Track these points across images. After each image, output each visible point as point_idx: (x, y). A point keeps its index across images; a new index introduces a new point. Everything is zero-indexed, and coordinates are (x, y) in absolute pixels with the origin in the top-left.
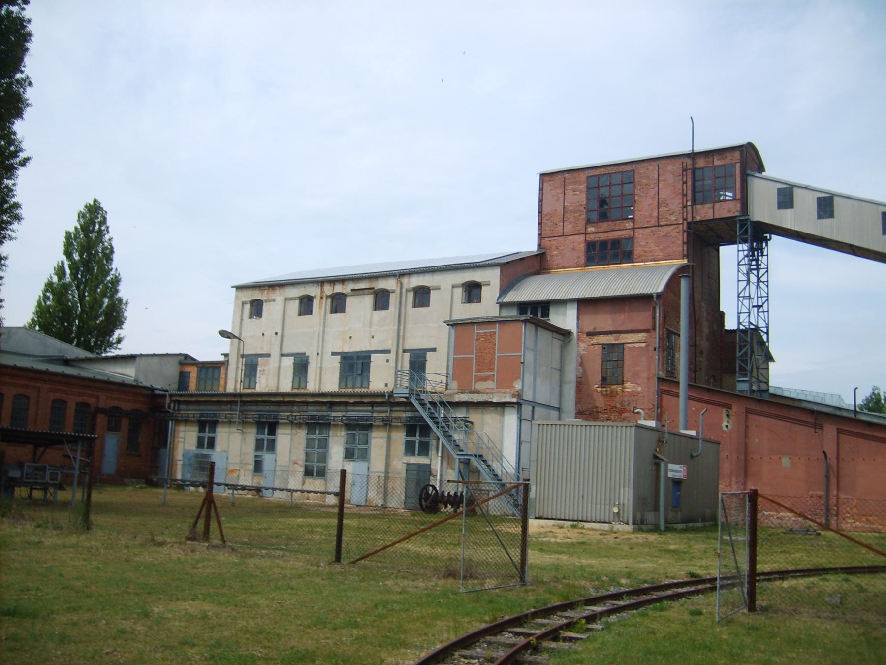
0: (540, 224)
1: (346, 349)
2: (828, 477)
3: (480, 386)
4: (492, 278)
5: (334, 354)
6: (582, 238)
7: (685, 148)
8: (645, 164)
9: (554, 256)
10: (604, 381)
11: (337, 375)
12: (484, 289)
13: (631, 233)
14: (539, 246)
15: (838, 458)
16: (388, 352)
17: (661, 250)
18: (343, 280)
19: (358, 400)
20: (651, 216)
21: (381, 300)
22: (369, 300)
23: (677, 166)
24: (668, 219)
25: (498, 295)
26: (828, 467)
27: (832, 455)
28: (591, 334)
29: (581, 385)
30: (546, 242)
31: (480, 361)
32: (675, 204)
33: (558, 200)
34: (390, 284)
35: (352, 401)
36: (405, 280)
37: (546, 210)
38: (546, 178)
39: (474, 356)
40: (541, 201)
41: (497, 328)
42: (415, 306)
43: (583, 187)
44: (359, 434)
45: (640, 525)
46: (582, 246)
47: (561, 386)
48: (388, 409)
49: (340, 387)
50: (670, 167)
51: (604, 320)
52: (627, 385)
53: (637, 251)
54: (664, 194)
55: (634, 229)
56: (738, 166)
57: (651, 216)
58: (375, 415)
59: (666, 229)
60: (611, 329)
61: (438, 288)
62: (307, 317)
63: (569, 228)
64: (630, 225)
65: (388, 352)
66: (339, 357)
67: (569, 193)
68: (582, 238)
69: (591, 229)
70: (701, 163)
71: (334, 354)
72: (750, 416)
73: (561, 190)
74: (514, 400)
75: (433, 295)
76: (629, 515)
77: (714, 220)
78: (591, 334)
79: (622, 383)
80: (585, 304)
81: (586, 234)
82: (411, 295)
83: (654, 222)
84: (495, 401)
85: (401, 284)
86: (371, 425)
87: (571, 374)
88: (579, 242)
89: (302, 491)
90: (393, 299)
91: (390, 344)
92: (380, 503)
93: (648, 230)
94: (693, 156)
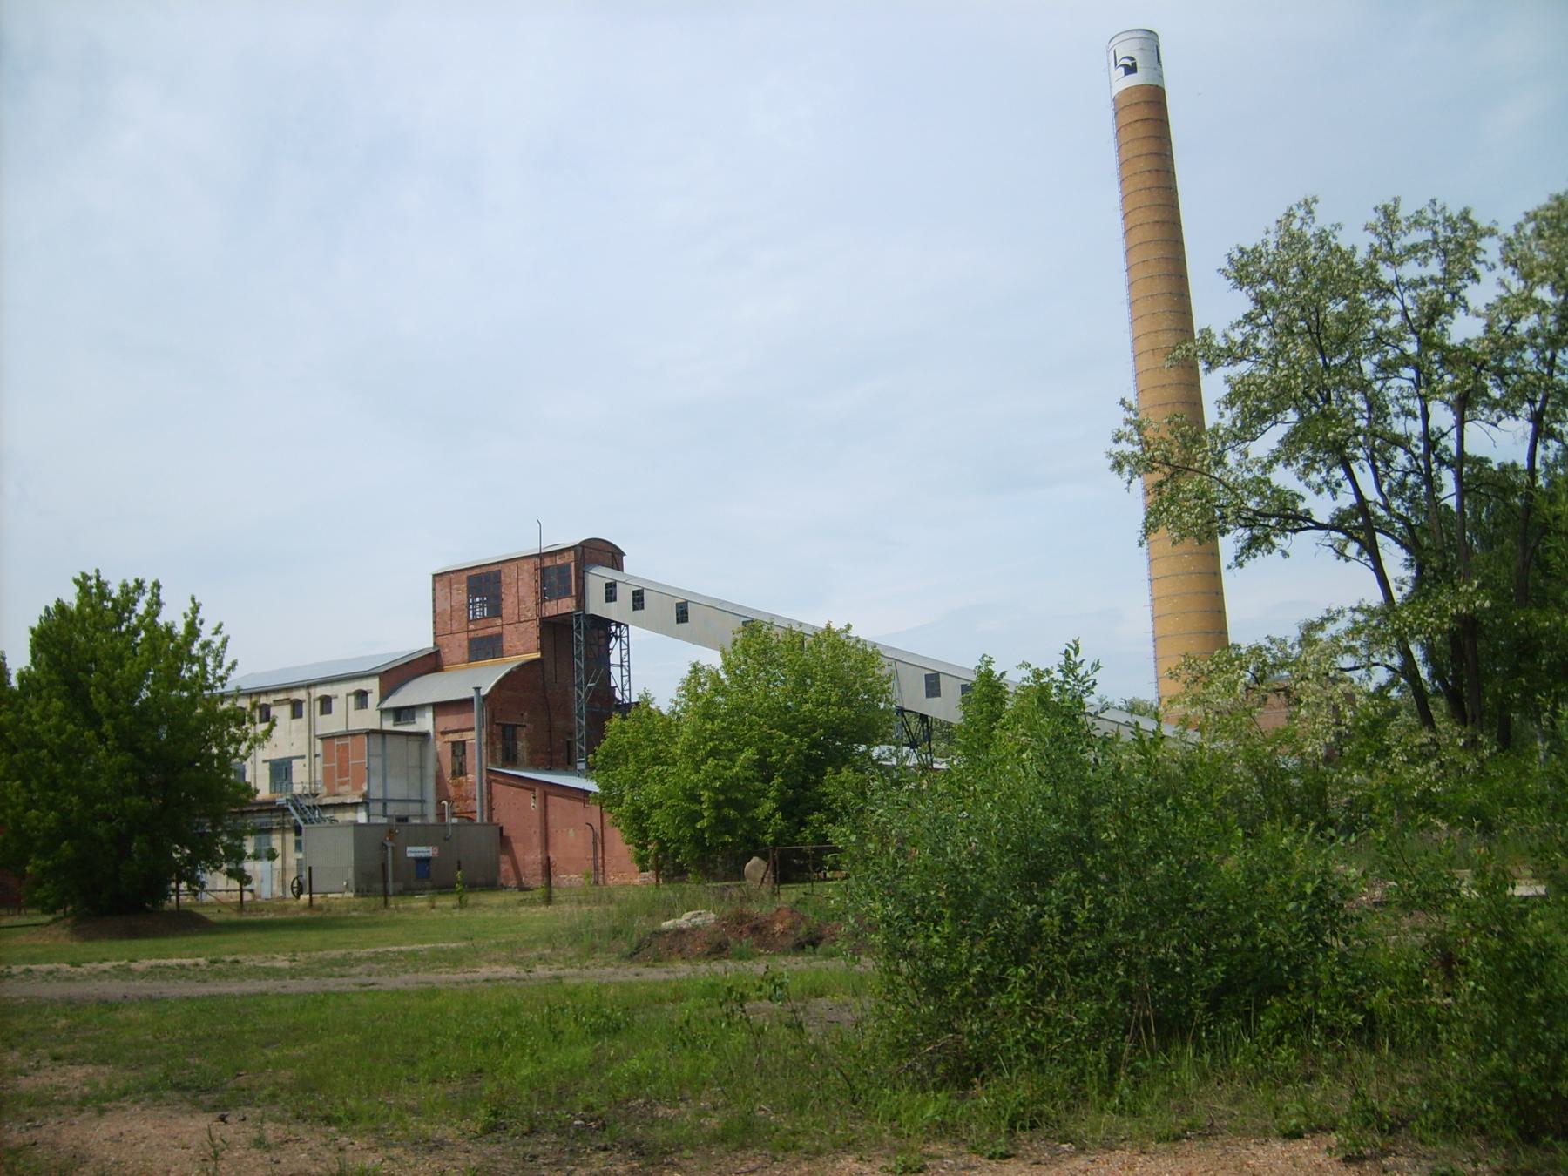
0: (434, 622)
1: (273, 757)
2: (595, 843)
3: (342, 789)
4: (373, 685)
5: (265, 761)
6: (464, 635)
7: (533, 549)
8: (508, 564)
9: (447, 657)
10: (454, 773)
11: (268, 781)
12: (333, 701)
13: (499, 629)
14: (435, 643)
15: (602, 827)
16: (303, 757)
17: (523, 645)
18: (266, 693)
19: (259, 808)
20: (514, 613)
21: (296, 709)
22: (287, 709)
23: (528, 567)
24: (526, 616)
25: (378, 702)
26: (595, 836)
27: (597, 826)
28: (444, 733)
29: (439, 778)
30: (442, 640)
31: (340, 767)
32: (530, 601)
33: (446, 599)
34: (300, 695)
35: (255, 809)
36: (312, 691)
37: (438, 610)
38: (437, 578)
39: (336, 764)
40: (434, 600)
41: (349, 740)
42: (356, 709)
43: (464, 586)
44: (264, 837)
45: (360, 892)
46: (466, 643)
47: (422, 780)
48: (281, 814)
49: (271, 792)
50: (526, 567)
51: (451, 721)
52: (469, 776)
53: (506, 646)
54: (523, 591)
55: (502, 625)
56: (573, 564)
57: (514, 613)
58: (274, 820)
59: (525, 624)
60: (456, 728)
61: (336, 697)
62: (684, 625)
63: (455, 626)
64: (499, 622)
65: (303, 757)
66: (268, 764)
67: (454, 592)
68: (464, 635)
69: (471, 627)
70: (548, 562)
71: (265, 761)
72: (549, 797)
73: (448, 590)
74: (360, 800)
75: (334, 702)
76: (352, 886)
77: (558, 615)
78: (444, 733)
79: (466, 774)
80: (440, 708)
81: (468, 631)
82: (318, 704)
83: (516, 619)
84: (348, 801)
85: (309, 694)
86: (271, 829)
87: (431, 770)
88: (462, 638)
89: (227, 891)
90: (305, 707)
91: (305, 751)
92: (281, 894)
93: (512, 626)
94: (541, 556)
